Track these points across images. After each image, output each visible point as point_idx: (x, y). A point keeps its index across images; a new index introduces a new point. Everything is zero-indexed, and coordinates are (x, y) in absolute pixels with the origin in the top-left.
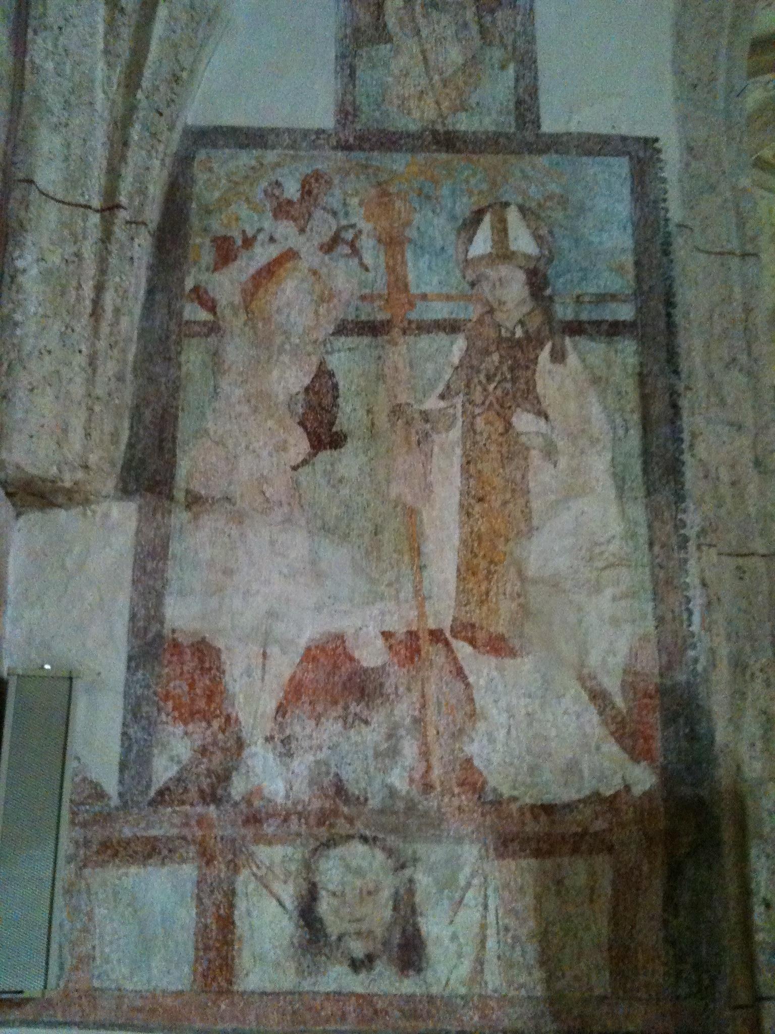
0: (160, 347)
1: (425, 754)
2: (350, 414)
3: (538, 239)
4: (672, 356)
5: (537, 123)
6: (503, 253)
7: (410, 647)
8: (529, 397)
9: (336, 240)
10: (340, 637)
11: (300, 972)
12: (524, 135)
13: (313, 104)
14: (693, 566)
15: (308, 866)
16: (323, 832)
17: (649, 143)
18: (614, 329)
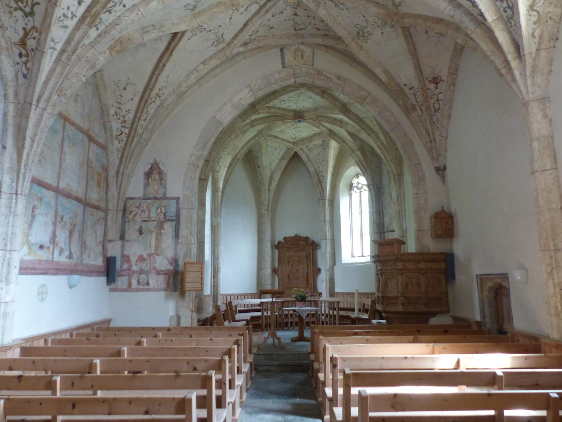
0: (123, 224)
4: (179, 224)
6: (161, 212)
7: (149, 255)
12: (164, 197)
17: (179, 198)
18: (173, 220)
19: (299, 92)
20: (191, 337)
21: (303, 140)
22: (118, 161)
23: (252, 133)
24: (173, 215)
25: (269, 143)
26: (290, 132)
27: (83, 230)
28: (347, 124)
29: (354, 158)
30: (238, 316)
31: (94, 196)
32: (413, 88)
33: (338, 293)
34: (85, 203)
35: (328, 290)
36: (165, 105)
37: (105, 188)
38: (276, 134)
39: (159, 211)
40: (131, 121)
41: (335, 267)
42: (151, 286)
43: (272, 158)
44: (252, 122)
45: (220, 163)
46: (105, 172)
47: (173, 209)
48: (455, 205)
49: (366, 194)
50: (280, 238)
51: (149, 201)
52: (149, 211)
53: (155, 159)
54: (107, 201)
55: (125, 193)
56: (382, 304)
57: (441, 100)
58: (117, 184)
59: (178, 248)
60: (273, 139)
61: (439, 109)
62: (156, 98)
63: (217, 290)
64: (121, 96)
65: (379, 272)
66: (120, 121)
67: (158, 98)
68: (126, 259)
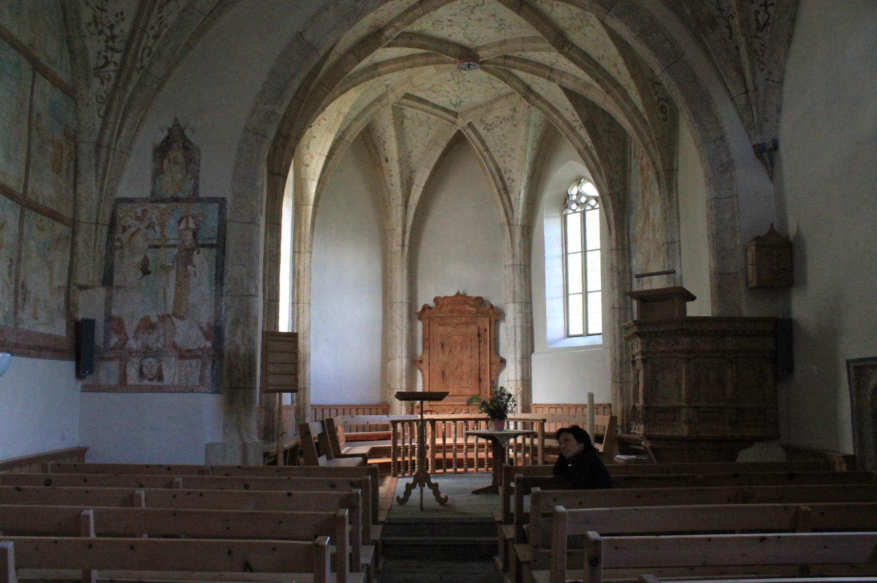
1: (165, 340)
2: (151, 267)
3: (196, 224)
4: (224, 253)
5: (198, 194)
6: (187, 228)
7: (163, 318)
9: (149, 226)
10: (148, 317)
12: (194, 198)
13: (144, 190)
14: (224, 300)
17: (224, 199)
20: (247, 487)
22: (98, 122)
24: (212, 234)
27: (19, 259)
28: (563, 73)
31: (45, 190)
34: (27, 204)
37: (71, 174)
39: (183, 226)
42: (167, 381)
45: (311, 149)
46: (73, 145)
47: (212, 220)
48: (796, 222)
49: (594, 217)
50: (426, 297)
51: (163, 206)
52: (162, 226)
53: (176, 120)
54: (76, 204)
58: (96, 171)
59: (223, 303)
61: (766, 24)
66: (103, 38)
68: (115, 323)
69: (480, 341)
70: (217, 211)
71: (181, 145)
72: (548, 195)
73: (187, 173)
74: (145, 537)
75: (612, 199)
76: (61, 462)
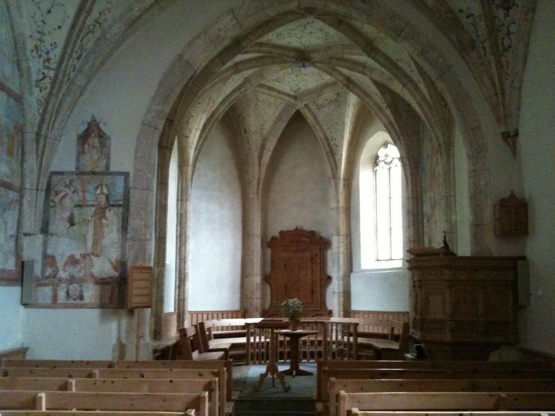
0: (46, 210)
2: (76, 220)
3: (108, 190)
4: (128, 211)
5: (109, 169)
6: (102, 193)
7: (84, 256)
8: (104, 217)
11: (67, 300)
12: (107, 172)
13: (71, 166)
14: (128, 244)
15: (68, 287)
16: (70, 282)
17: (128, 173)
18: (119, 206)
19: (304, 21)
20: (142, 376)
21: (309, 92)
22: (38, 118)
23: (236, 81)
25: (262, 97)
26: (291, 80)
28: (372, 70)
29: (381, 119)
30: (213, 344)
32: (472, 15)
33: (355, 312)
35: (341, 307)
36: (108, 36)
37: (20, 156)
38: (271, 84)
39: (98, 192)
40: (57, 59)
41: (352, 275)
43: (264, 119)
44: (236, 65)
49: (397, 170)
50: (274, 232)
53: (93, 116)
54: (22, 176)
55: (48, 165)
56: (421, 330)
57: (513, 33)
60: (266, 91)
61: (510, 46)
62: (94, 26)
63: (184, 304)
64: (44, 22)
65: (417, 283)
66: (42, 60)
67: (98, 25)
68: (49, 260)
69: (313, 263)
70: (123, 181)
71: (97, 134)
72: (365, 156)
73: (102, 154)
74: (74, 411)
75: (409, 161)
76: (11, 358)
